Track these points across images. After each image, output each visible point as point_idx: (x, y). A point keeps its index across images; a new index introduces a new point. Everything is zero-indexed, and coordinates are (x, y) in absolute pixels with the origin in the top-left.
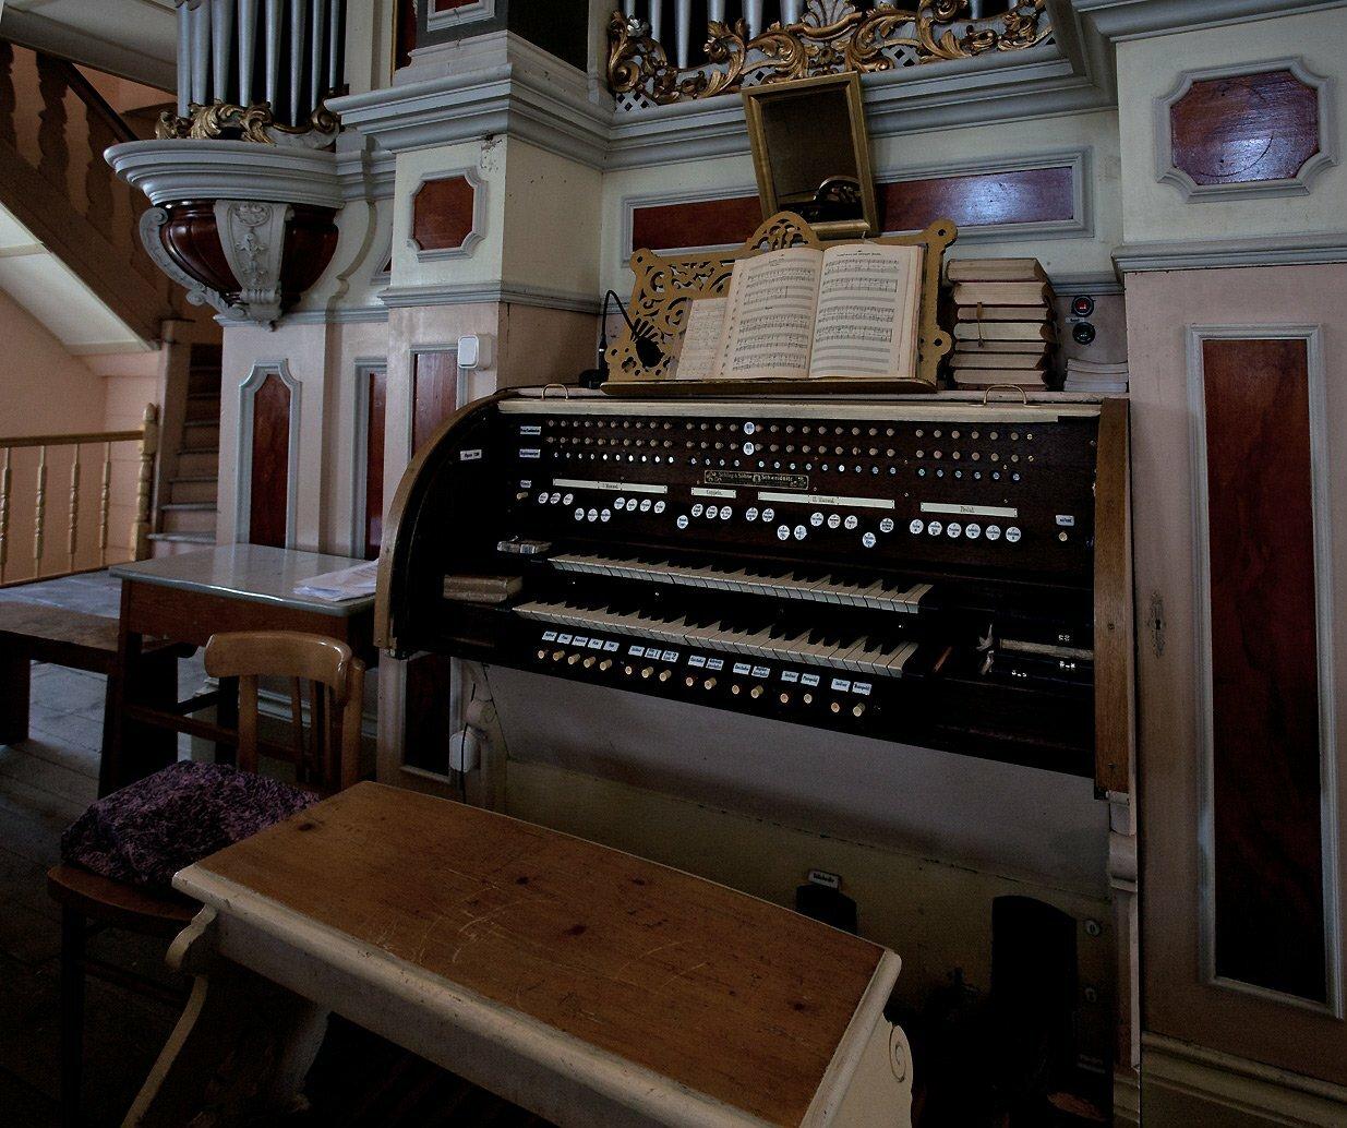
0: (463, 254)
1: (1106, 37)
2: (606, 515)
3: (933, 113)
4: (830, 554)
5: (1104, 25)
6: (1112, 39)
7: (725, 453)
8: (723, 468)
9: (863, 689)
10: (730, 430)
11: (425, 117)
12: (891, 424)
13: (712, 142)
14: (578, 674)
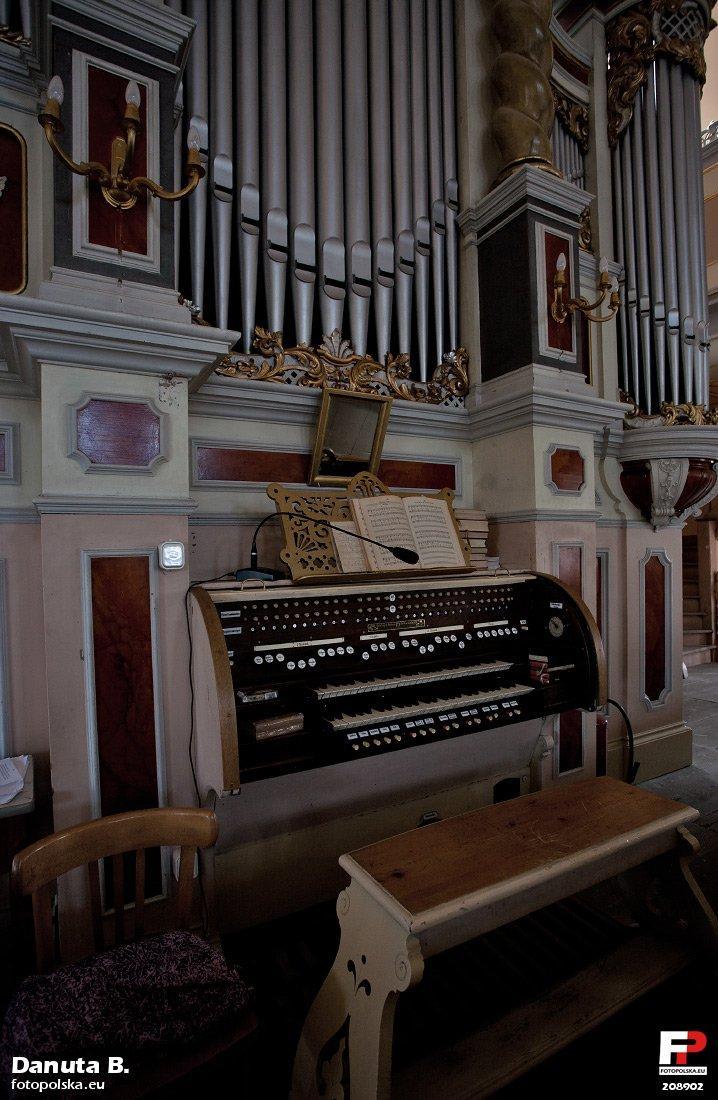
0: (148, 473)
1: (35, 358)
2: (312, 662)
3: (406, 426)
4: (447, 656)
5: (33, 350)
6: (39, 361)
7: (379, 615)
8: (377, 621)
9: (514, 704)
10: (381, 600)
11: (39, 333)
12: (463, 589)
13: (275, 413)
14: (385, 748)
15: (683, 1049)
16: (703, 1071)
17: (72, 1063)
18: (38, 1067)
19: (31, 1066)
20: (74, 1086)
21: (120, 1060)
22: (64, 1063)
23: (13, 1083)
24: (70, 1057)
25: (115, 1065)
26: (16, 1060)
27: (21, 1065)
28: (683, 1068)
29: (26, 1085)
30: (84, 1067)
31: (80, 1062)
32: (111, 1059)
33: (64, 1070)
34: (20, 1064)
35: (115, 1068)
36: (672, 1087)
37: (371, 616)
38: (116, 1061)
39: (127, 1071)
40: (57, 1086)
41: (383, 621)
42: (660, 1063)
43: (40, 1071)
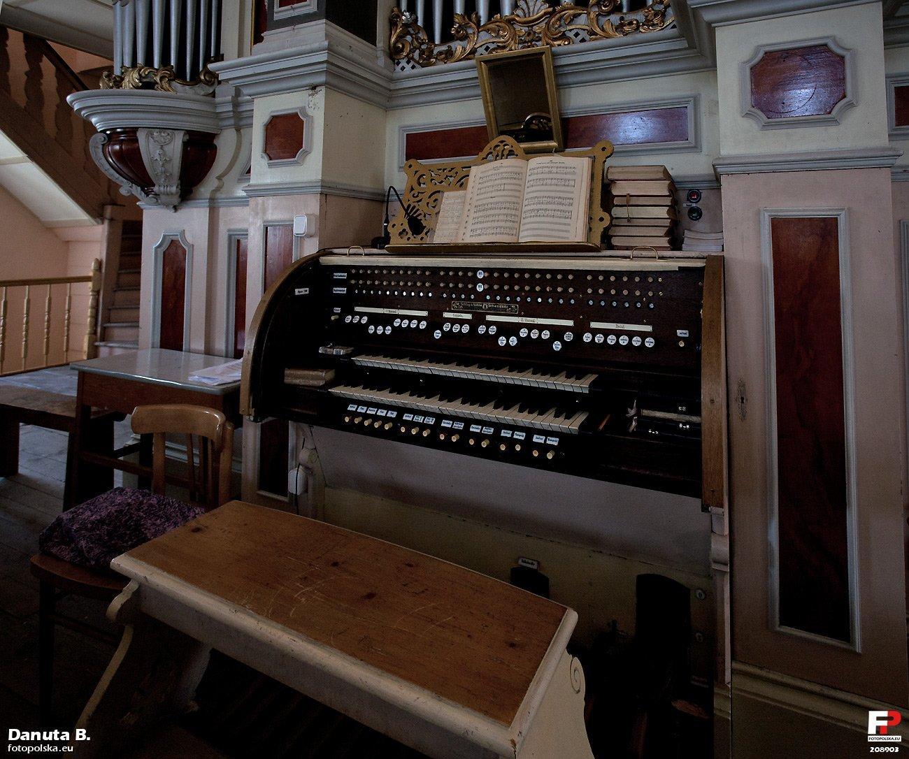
8: (464, 300)
10: (468, 275)
15: (885, 723)
16: (898, 738)
17: (51, 733)
18: (27, 736)
19: (21, 735)
20: (52, 749)
21: (84, 731)
22: (45, 733)
23: (9, 747)
24: (50, 729)
25: (81, 734)
26: (11, 731)
27: (14, 734)
28: (884, 737)
29: (18, 748)
30: (59, 736)
31: (56, 732)
32: (78, 731)
33: (45, 738)
34: (14, 734)
35: (81, 737)
36: (892, 750)
37: (459, 292)
38: (81, 732)
39: (89, 739)
40: (40, 749)
41: (496, 301)
42: (869, 733)
43: (28, 739)
